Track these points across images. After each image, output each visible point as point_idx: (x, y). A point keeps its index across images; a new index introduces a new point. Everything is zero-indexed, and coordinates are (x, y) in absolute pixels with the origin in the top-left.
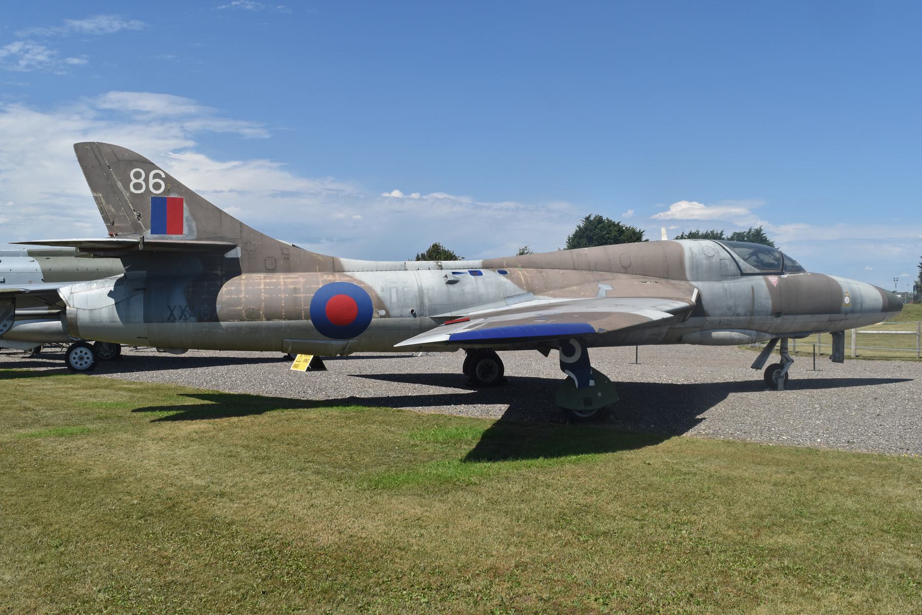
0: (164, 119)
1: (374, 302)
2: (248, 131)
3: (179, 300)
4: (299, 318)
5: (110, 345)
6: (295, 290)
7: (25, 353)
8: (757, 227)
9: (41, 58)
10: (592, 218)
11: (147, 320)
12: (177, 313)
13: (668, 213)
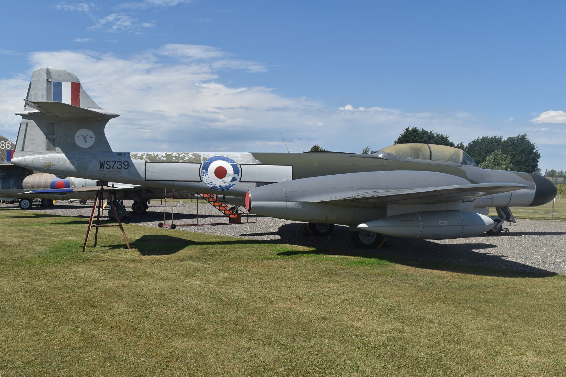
0: (199, 61)
1: (71, 183)
2: (254, 67)
3: (12, 182)
4: (47, 188)
5: (48, 200)
6: (47, 179)
7: (12, 202)
8: (522, 134)
9: (128, 23)
10: (410, 129)
11: (3, 188)
12: (11, 186)
13: (538, 119)
